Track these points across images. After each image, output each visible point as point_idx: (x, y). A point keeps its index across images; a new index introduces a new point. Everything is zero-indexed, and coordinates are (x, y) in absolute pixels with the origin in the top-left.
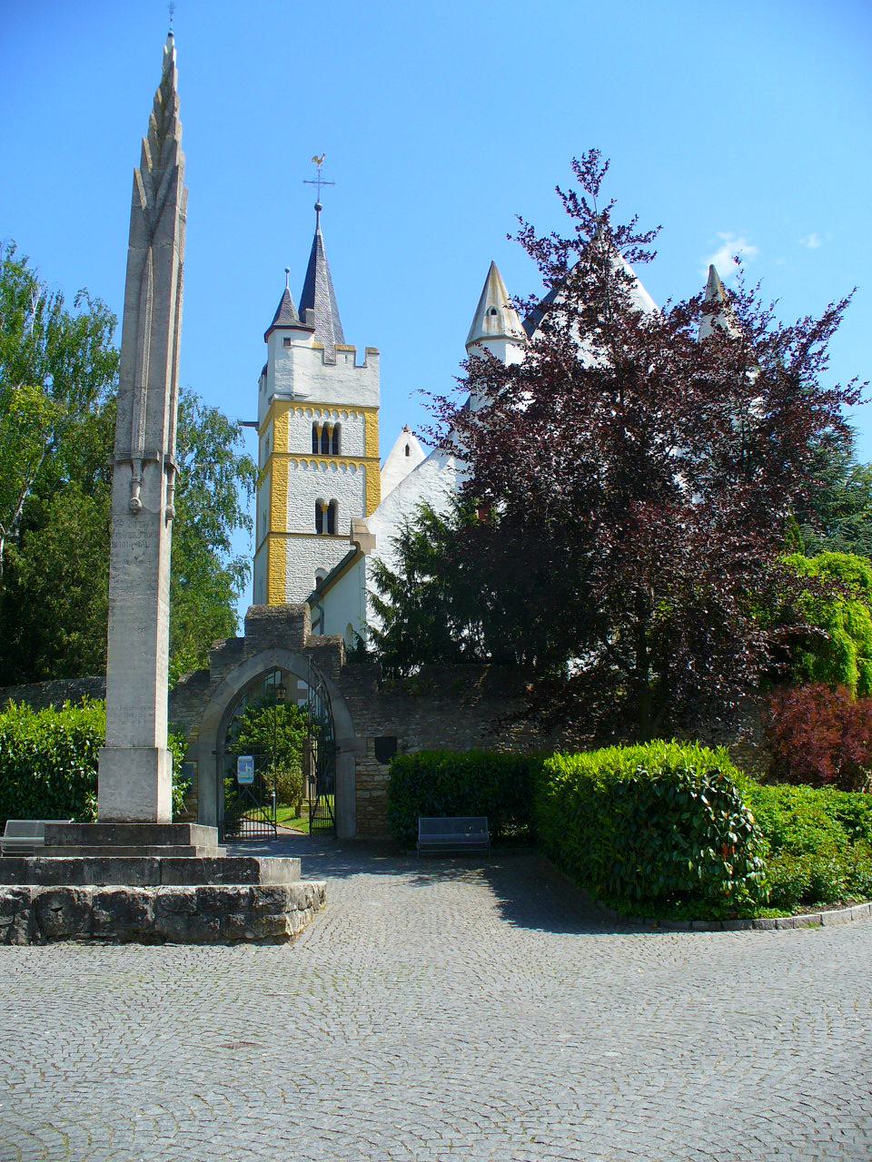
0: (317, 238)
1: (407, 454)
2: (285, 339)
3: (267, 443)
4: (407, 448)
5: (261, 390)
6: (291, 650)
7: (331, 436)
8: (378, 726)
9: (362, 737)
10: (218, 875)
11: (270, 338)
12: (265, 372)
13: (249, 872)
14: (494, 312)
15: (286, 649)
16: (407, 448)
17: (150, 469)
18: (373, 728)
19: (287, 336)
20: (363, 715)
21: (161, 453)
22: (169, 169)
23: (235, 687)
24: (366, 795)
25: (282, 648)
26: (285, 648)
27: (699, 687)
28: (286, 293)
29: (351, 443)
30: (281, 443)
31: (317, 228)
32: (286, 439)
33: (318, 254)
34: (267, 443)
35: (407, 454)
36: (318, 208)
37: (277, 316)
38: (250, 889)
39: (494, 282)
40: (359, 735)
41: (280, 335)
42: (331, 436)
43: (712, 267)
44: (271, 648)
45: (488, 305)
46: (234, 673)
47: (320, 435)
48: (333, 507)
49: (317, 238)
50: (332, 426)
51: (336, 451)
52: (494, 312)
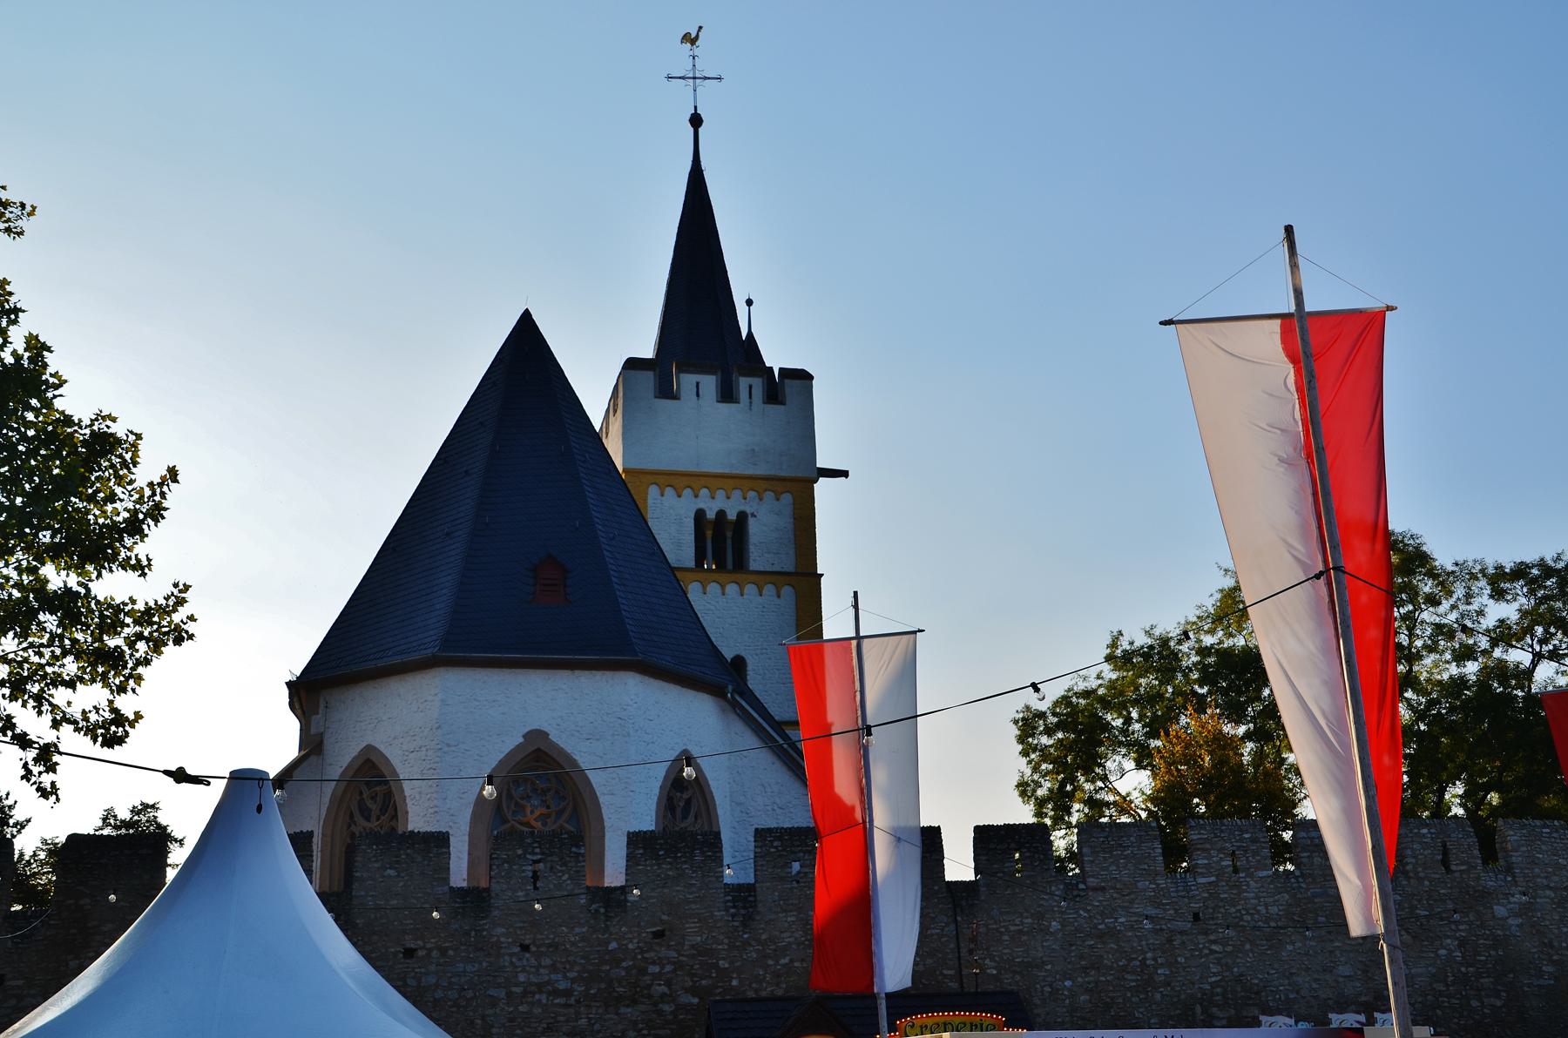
42: (729, 534)
47: (709, 533)
50: (732, 515)
51: (740, 564)
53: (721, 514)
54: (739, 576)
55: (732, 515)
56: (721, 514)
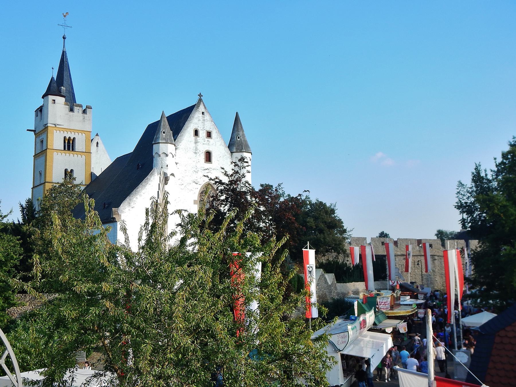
0: (64, 54)
4: (97, 143)
7: (71, 142)
16: (97, 143)
27: (414, 326)
29: (79, 145)
30: (50, 145)
36: (64, 38)
41: (51, 98)
42: (71, 142)
43: (237, 113)
47: (67, 142)
49: (64, 54)
50: (72, 138)
51: (73, 150)
53: (69, 138)
55: (72, 138)
56: (69, 138)
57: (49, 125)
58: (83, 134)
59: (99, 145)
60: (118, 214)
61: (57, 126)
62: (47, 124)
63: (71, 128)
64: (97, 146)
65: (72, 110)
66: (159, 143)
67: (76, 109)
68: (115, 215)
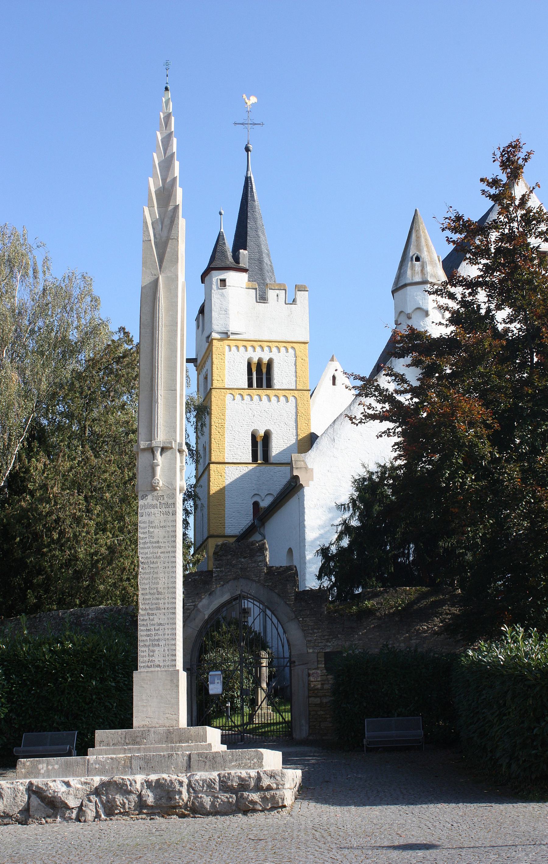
0: (248, 180)
1: (334, 384)
2: (221, 280)
3: (206, 378)
4: (334, 378)
5: (198, 327)
6: (252, 580)
7: (264, 370)
8: (327, 642)
9: (313, 652)
10: (233, 764)
11: (207, 279)
12: (202, 311)
13: (255, 760)
14: (418, 259)
15: (249, 579)
16: (334, 378)
17: (168, 454)
18: (323, 644)
19: (222, 277)
20: (314, 633)
21: (176, 441)
22: (171, 208)
23: (205, 613)
24: (317, 701)
25: (244, 578)
26: (248, 578)
28: (220, 237)
30: (219, 378)
31: (248, 170)
32: (224, 375)
33: (249, 198)
34: (206, 378)
35: (334, 384)
36: (247, 150)
37: (213, 258)
38: (258, 772)
39: (418, 238)
40: (311, 651)
41: (216, 276)
42: (264, 370)
44: (236, 579)
45: (412, 252)
46: (205, 601)
48: (267, 436)
49: (248, 180)
50: (265, 361)
51: (269, 385)
52: (418, 259)
54: (268, 392)
57: (215, 335)
58: (290, 350)
59: (337, 382)
60: (306, 468)
61: (232, 337)
62: (211, 334)
63: (261, 339)
64: (277, 301)
65: (262, 298)
66: (405, 285)
67: (271, 294)
68: (297, 468)
